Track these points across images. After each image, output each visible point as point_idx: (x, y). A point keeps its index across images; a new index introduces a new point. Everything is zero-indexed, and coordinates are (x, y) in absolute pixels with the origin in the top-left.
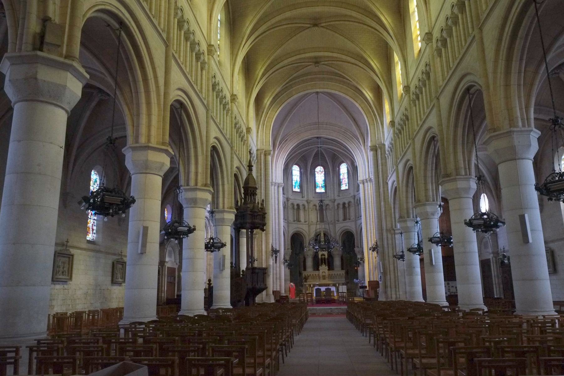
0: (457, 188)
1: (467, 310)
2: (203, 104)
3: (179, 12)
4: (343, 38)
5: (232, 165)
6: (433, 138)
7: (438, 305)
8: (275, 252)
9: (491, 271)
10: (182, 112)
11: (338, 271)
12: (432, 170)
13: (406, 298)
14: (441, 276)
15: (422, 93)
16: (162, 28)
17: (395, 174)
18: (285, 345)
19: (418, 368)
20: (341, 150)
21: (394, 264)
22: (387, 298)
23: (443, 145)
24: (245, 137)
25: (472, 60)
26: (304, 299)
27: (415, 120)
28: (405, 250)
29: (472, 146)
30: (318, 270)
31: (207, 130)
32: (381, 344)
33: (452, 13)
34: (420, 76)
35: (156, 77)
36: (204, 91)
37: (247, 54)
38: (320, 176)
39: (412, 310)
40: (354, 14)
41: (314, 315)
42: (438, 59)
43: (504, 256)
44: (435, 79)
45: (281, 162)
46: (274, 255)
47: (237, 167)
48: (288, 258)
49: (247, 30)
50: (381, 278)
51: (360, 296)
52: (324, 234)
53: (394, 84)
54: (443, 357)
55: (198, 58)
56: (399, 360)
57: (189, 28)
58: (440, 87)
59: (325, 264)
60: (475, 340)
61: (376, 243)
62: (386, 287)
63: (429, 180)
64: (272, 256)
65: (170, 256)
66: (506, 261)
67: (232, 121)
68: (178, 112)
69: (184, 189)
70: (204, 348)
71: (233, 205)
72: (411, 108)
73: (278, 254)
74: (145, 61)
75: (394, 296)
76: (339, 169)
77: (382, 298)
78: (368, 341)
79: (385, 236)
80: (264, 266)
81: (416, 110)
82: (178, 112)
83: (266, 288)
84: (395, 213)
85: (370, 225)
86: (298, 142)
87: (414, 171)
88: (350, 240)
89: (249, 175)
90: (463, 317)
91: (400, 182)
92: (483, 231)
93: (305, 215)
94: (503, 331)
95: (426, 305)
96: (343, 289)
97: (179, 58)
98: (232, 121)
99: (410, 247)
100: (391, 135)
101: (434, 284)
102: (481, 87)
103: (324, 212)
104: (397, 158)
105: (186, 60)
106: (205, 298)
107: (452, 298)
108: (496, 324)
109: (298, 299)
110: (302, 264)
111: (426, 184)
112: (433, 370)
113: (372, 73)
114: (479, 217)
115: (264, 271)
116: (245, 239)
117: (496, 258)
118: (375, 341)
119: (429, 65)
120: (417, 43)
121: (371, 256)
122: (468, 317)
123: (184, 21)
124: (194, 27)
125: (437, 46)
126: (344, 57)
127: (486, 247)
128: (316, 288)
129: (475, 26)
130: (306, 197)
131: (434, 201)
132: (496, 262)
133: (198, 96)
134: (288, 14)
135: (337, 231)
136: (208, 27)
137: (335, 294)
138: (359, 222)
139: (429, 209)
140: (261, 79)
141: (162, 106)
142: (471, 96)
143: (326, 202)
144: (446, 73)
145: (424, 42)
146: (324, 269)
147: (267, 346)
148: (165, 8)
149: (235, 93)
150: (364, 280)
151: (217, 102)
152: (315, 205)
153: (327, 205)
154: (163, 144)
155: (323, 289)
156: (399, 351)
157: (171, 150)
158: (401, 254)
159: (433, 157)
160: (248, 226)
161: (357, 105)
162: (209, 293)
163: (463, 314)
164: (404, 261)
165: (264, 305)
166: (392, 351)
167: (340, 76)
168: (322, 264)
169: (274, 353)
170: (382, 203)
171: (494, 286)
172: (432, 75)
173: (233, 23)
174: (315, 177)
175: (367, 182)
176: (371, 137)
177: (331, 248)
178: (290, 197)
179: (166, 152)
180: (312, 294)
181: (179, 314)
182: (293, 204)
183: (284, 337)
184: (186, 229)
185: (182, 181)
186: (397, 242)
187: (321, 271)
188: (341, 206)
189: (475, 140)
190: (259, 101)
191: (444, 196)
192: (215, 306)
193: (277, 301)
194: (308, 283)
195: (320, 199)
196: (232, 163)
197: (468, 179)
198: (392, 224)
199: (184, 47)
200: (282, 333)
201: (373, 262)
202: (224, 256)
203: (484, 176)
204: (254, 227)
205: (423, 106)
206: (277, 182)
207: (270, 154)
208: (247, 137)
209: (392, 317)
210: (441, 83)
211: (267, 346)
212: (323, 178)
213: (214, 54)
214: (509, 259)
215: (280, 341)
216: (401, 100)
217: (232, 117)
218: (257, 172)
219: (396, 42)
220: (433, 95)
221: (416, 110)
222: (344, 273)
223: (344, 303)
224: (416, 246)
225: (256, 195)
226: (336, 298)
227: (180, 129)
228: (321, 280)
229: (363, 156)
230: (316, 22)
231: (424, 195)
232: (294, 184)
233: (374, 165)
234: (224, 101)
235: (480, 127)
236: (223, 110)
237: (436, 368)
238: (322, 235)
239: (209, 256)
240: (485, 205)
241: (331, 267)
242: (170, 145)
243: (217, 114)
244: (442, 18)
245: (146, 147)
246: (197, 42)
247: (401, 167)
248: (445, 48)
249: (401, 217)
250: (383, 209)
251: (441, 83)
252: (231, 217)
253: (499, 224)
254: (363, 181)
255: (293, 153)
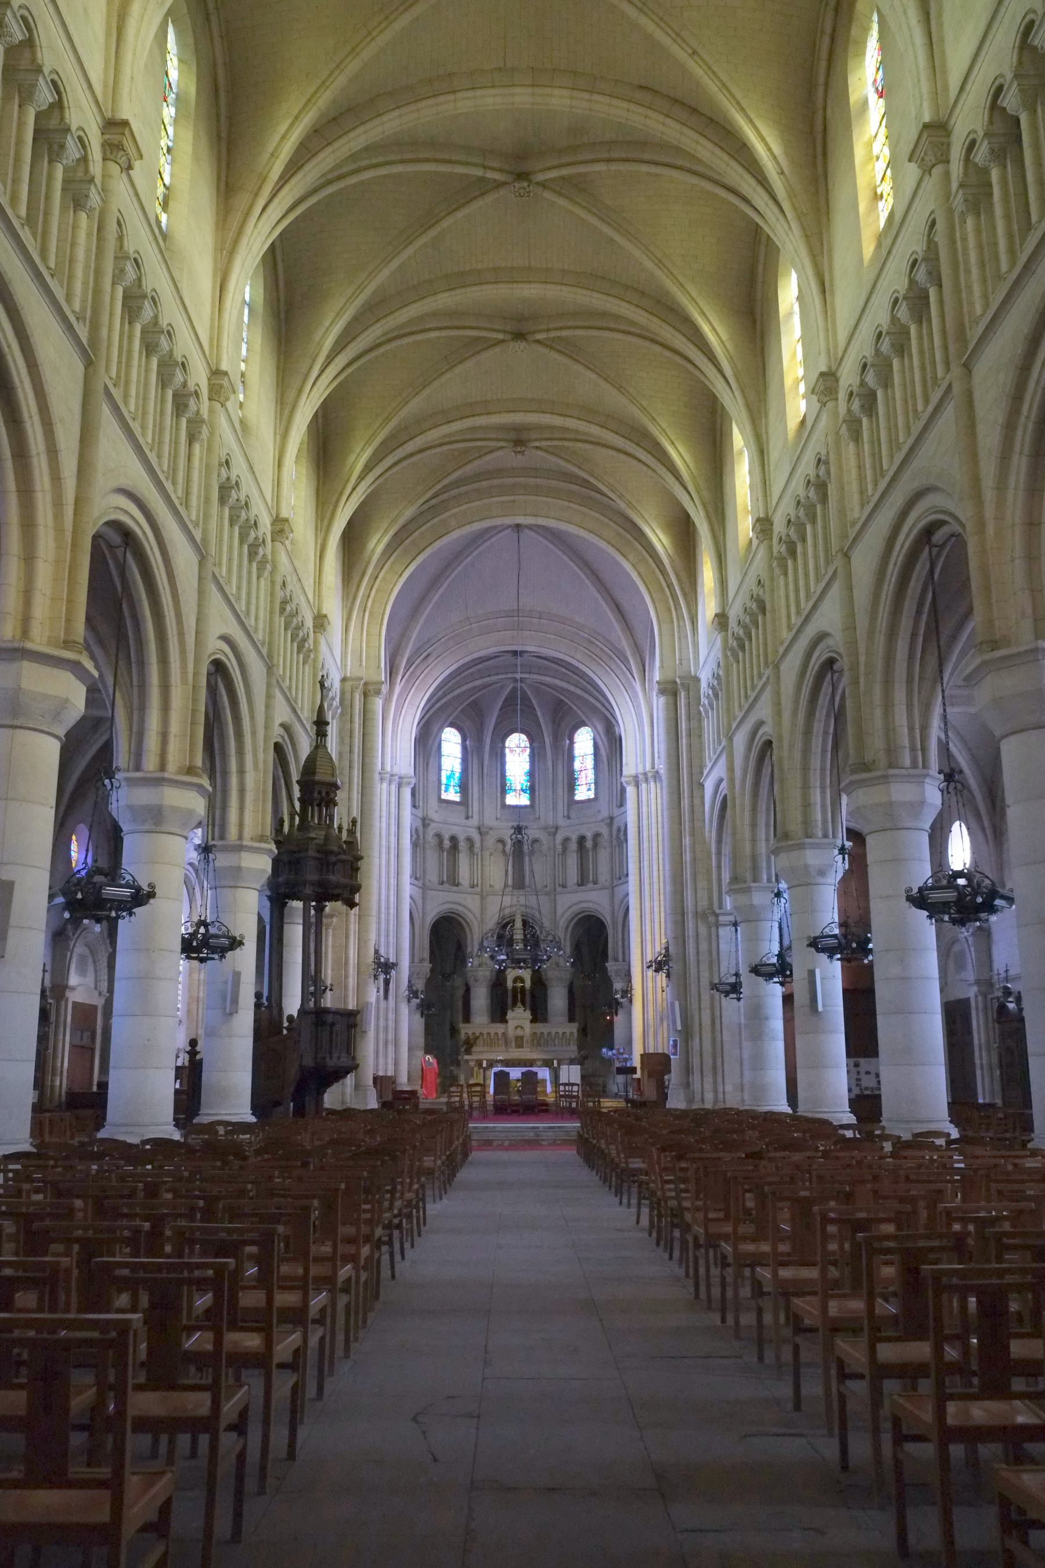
0: (891, 804)
1: (906, 1136)
2: (192, 539)
3: (129, 268)
4: (594, 376)
5: (268, 718)
6: (830, 663)
7: (826, 1123)
8: (385, 967)
9: (970, 1032)
10: (129, 556)
11: (561, 1026)
12: (824, 751)
13: (743, 1101)
14: (838, 1042)
15: (804, 540)
16: (77, 308)
17: (723, 762)
18: (399, 1226)
19: (769, 1294)
20: (579, 692)
21: (712, 1008)
22: (690, 1100)
23: (856, 682)
24: (311, 640)
25: (942, 453)
26: (461, 1102)
27: (784, 612)
28: (744, 971)
29: (933, 689)
30: (503, 1020)
31: (199, 612)
32: (667, 1227)
33: (894, 320)
34: (801, 492)
35: (52, 451)
36: (194, 501)
37: (324, 404)
38: (517, 757)
39: (757, 1134)
40: (626, 310)
41: (487, 1144)
42: (852, 447)
43: (1007, 992)
44: (841, 500)
45: (410, 718)
46: (382, 977)
47: (282, 725)
48: (420, 985)
49: (324, 337)
50: (675, 1045)
51: (616, 1096)
52: (525, 923)
53: (729, 512)
54: (835, 1263)
55: (180, 403)
56: (715, 1271)
57: (156, 317)
58: (854, 524)
59: (523, 1003)
60: (923, 1214)
61: (667, 949)
62: (687, 1070)
63: (815, 781)
64: (376, 977)
65: (82, 971)
66: (1011, 1006)
67: (272, 594)
68: (115, 557)
69: (127, 779)
70: (156, 1233)
71: (268, 831)
72: (772, 579)
73: (393, 972)
74: (23, 403)
75: (709, 1096)
76: (572, 743)
77: (676, 1101)
78: (635, 1218)
79: (690, 931)
80: (351, 1006)
81: (787, 585)
82: (115, 557)
83: (353, 1067)
84: (719, 867)
85: (652, 900)
86: (461, 663)
87: (775, 751)
88: (595, 942)
89: (317, 747)
90: (893, 1155)
91: (737, 782)
92: (954, 921)
93: (471, 865)
94: (1000, 1192)
95: (796, 1120)
96: (571, 1074)
97: (143, 435)
98: (272, 594)
99: (756, 961)
100: (717, 652)
101: (819, 1064)
102: (963, 526)
103: (527, 859)
104: (730, 716)
105: (144, 408)
106: (177, 1092)
107: (867, 1104)
108: (982, 1172)
109: (444, 1099)
110: (460, 1003)
111: (806, 787)
112: (808, 1298)
113: (670, 480)
114: (944, 882)
115: (350, 1021)
116: (300, 928)
117: (985, 996)
118: (651, 1222)
119: (827, 463)
120: (796, 403)
121: (650, 984)
122: (905, 1154)
123: (144, 296)
124: (170, 314)
125: (849, 411)
126: (595, 430)
127: (961, 966)
128: (495, 1069)
129: (951, 357)
130: (476, 816)
131: (825, 836)
132: (985, 1008)
133: (176, 513)
134: (444, 300)
135: (559, 912)
136: (212, 320)
137: (549, 1088)
138: (619, 891)
139: (812, 858)
140: (361, 478)
141: (69, 535)
142: (935, 551)
143: (533, 832)
144: (870, 487)
145: (815, 398)
146: (519, 1017)
147: (345, 1230)
148: (88, 251)
149: (284, 514)
150: (631, 1053)
151: (231, 537)
152: (501, 841)
153: (535, 841)
154: (67, 644)
155: (515, 1073)
156: (716, 1247)
157: (89, 665)
158: (733, 980)
159: (828, 715)
160: (308, 890)
161: (627, 566)
162: (191, 1076)
163: (894, 1145)
164: (739, 999)
165: (347, 1114)
166: (697, 1246)
167: (585, 484)
168: (514, 1004)
169: (365, 1251)
170: (687, 841)
171: (978, 1073)
172: (832, 490)
173: (288, 311)
174: (503, 764)
175: (647, 780)
176: (662, 661)
177: (542, 961)
178: (432, 815)
179: (76, 668)
180: (484, 1086)
181: (101, 1135)
182: (439, 836)
183: (398, 1203)
184: (127, 892)
185: (122, 757)
186: (723, 947)
187: (512, 1024)
188: (573, 846)
189: (941, 672)
190: (353, 540)
191: (853, 825)
192: (204, 1118)
193: (384, 1105)
194: (474, 1057)
195: (515, 824)
196: (269, 714)
197: (919, 780)
198: (710, 898)
199: (142, 373)
200: (392, 1192)
201: (655, 1000)
202: (237, 975)
203: (961, 772)
204: (324, 894)
205: (806, 575)
206: (396, 771)
207: (378, 692)
208: (315, 642)
209: (701, 1150)
210: (856, 514)
211: (345, 1230)
212: (526, 767)
213: (227, 399)
214: (1019, 1000)
215: (387, 1215)
216: (746, 556)
217: (273, 582)
218: (341, 742)
219: (737, 393)
220: (835, 545)
221: (787, 585)
222: (575, 1031)
223: (572, 1113)
224: (774, 960)
225: (335, 804)
226: (551, 1099)
227: (120, 609)
228: (510, 1048)
229: (637, 707)
230: (520, 328)
231: (800, 819)
232: (444, 780)
233: (668, 733)
234: (253, 535)
235: (954, 637)
236: (250, 561)
237: (815, 1293)
238: (519, 924)
239: (195, 976)
240: (960, 851)
241: (539, 1014)
242: (87, 647)
243: (229, 570)
244: (866, 332)
245: (16, 650)
246: (180, 360)
247: (740, 740)
248: (870, 416)
249: (735, 879)
250: (688, 857)
251: (856, 513)
252: (260, 864)
253: (998, 902)
254: (636, 777)
255: (445, 695)
